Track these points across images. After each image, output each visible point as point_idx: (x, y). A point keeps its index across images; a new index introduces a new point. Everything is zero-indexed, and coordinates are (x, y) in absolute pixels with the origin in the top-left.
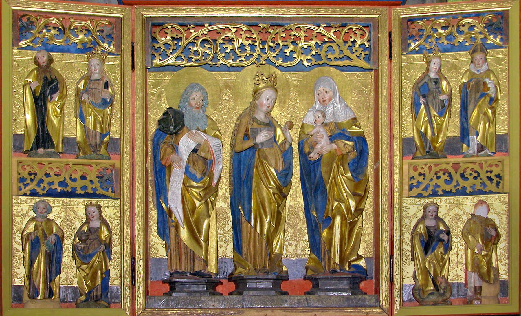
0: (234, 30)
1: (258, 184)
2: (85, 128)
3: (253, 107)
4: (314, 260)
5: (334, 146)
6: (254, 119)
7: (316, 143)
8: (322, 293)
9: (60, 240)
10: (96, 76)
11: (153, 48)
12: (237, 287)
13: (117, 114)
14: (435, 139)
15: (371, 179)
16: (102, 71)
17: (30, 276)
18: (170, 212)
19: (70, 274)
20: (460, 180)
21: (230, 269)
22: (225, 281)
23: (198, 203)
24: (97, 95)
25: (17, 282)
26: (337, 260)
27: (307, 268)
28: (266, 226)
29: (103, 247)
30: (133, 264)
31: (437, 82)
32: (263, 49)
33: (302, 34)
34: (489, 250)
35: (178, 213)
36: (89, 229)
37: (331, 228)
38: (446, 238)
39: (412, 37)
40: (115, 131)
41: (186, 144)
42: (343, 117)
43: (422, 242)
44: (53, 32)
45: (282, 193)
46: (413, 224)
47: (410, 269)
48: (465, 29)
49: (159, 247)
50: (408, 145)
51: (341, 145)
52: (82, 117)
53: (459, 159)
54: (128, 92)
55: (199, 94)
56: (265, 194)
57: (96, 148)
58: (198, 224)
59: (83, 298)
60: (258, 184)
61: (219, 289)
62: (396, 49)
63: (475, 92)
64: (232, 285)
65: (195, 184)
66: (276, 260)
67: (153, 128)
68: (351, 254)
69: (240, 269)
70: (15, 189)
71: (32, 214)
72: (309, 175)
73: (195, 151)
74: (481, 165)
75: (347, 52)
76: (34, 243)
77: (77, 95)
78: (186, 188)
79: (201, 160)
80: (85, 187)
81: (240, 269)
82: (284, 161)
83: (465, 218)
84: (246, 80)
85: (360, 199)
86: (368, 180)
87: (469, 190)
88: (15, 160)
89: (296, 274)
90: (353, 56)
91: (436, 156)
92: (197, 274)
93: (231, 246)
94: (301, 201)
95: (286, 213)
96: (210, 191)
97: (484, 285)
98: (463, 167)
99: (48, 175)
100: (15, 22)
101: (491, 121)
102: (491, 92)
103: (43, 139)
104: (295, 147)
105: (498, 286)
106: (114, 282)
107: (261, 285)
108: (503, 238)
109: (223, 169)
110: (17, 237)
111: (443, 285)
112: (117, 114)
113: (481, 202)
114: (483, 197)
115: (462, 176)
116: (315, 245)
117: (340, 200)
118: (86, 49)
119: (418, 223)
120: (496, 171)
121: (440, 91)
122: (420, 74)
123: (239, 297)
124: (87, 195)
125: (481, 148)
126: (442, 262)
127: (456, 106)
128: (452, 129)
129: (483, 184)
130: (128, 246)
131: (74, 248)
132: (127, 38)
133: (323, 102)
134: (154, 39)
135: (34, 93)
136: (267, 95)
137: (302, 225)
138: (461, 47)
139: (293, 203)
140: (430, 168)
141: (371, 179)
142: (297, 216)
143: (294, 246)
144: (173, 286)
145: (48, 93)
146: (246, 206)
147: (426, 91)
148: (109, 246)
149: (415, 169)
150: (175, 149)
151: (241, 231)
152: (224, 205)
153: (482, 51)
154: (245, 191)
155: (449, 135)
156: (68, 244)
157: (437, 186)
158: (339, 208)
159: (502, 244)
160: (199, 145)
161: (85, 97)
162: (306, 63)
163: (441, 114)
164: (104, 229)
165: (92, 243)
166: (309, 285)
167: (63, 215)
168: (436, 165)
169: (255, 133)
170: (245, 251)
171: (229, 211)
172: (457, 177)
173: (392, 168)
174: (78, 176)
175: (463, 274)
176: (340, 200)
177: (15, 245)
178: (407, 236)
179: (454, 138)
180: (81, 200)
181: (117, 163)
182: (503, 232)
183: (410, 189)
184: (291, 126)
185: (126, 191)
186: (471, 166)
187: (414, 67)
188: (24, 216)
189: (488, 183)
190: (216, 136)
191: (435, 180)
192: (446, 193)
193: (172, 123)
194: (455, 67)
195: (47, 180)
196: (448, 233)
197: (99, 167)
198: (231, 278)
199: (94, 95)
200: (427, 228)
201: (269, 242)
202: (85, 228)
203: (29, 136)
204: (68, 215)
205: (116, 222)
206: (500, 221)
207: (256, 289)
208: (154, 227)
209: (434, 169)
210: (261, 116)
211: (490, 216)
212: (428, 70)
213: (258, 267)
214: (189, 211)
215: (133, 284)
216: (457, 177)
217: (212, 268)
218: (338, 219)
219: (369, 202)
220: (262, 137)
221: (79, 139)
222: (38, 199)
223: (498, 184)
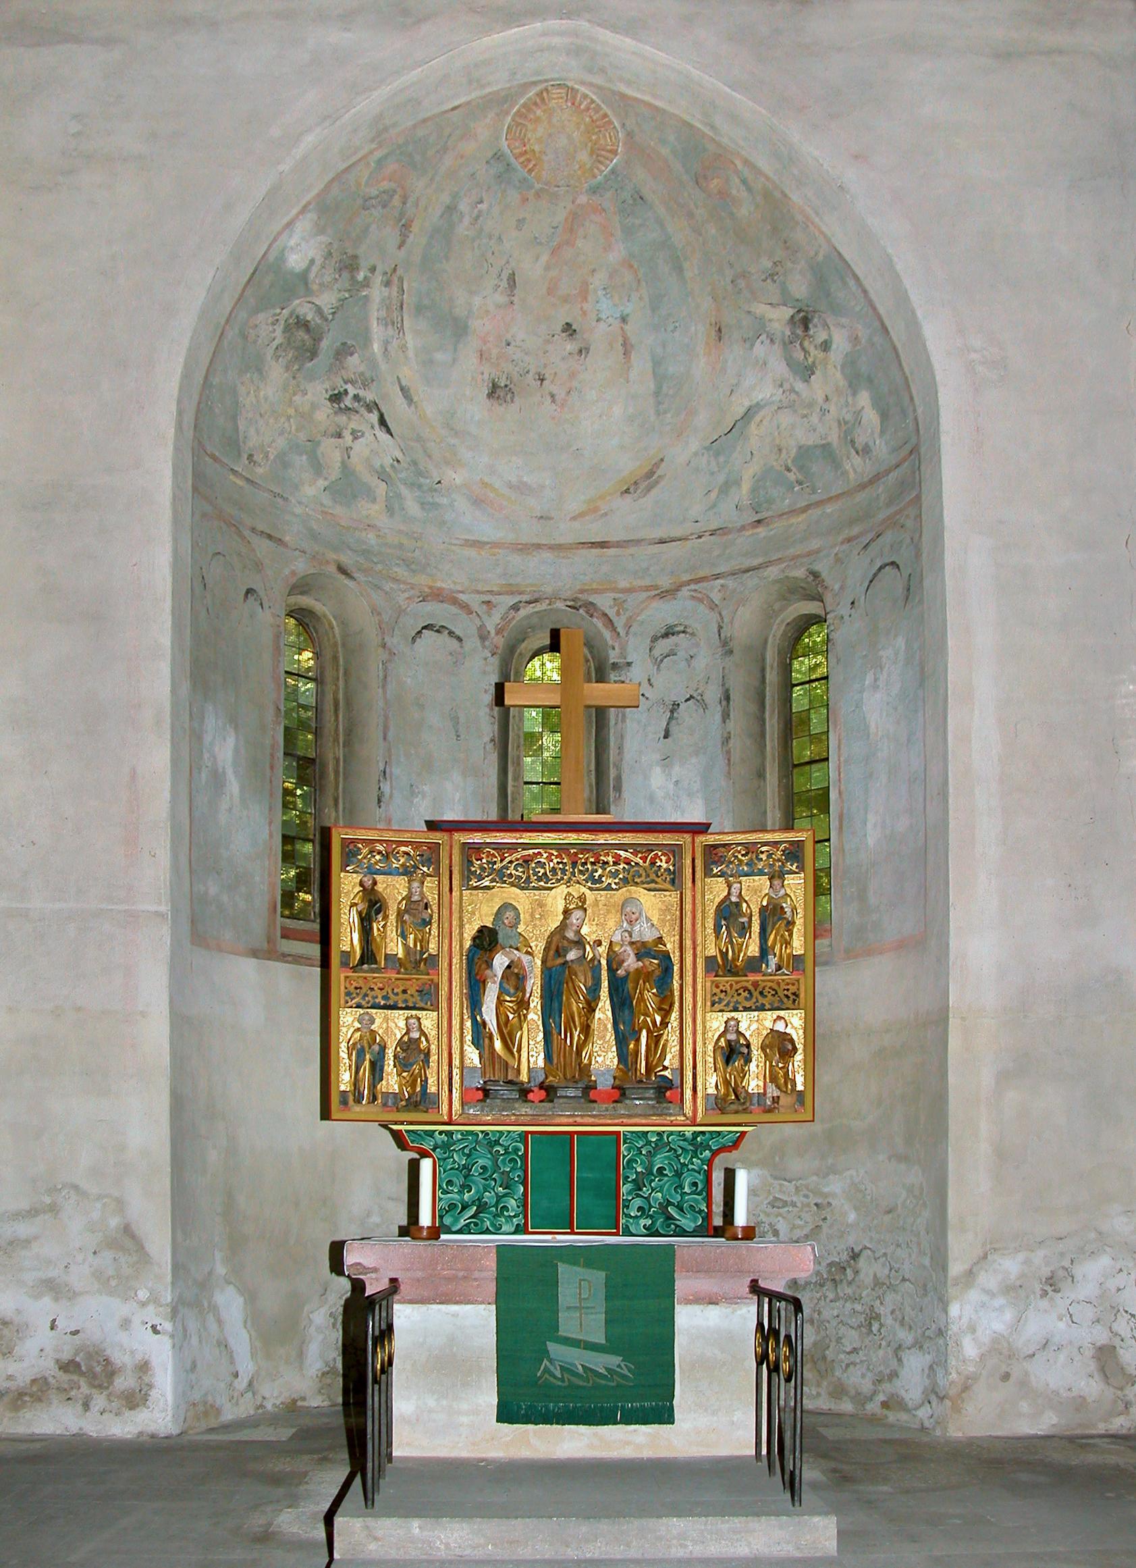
0: (545, 855)
1: (568, 999)
2: (405, 945)
3: (563, 926)
4: (621, 1070)
5: (640, 964)
6: (564, 938)
7: (623, 961)
8: (628, 1102)
9: (383, 1048)
10: (415, 898)
11: (467, 875)
12: (548, 1095)
13: (434, 931)
14: (736, 958)
15: (677, 993)
16: (422, 893)
17: (356, 1083)
18: (484, 1024)
19: (392, 1082)
20: (760, 997)
21: (541, 1079)
22: (536, 1089)
23: (511, 1016)
24: (416, 914)
25: (343, 1088)
26: (643, 1071)
27: (615, 1078)
28: (576, 1038)
29: (422, 1056)
30: (450, 1073)
31: (738, 905)
32: (573, 874)
33: (610, 859)
34: (786, 1063)
35: (492, 1025)
36: (410, 1039)
37: (638, 1040)
38: (746, 1051)
39: (715, 863)
40: (433, 947)
41: (500, 962)
42: (649, 936)
43: (723, 1054)
44: (378, 857)
45: (591, 1008)
46: (716, 1037)
47: (713, 1079)
48: (764, 857)
49: (473, 1056)
50: (710, 961)
51: (647, 963)
52: (404, 936)
53: (759, 978)
54: (446, 912)
55: (512, 914)
56: (575, 1009)
57: (417, 964)
58: (512, 1036)
59: (404, 1103)
60: (568, 999)
61: (531, 1096)
62: (699, 875)
63: (773, 914)
64: (543, 1092)
65: (508, 998)
66: (585, 1070)
67: (468, 944)
68: (657, 1066)
69: (551, 1078)
70: (342, 1002)
71: (357, 1025)
72: (617, 990)
73: (509, 967)
74: (779, 984)
75: (653, 876)
76: (358, 1051)
77: (398, 915)
78: (500, 1002)
79: (515, 977)
80: (406, 1001)
81: (551, 1078)
82: (593, 977)
83: (765, 1033)
84: (556, 899)
85: (666, 1014)
86: (672, 994)
87: (767, 1006)
88: (342, 976)
89: (605, 1083)
90: (659, 880)
91: (736, 974)
92: (510, 1082)
93: (542, 1055)
94: (610, 1014)
95: (595, 1025)
96: (523, 1004)
97: (782, 1096)
98: (762, 984)
99: (372, 989)
100: (343, 848)
101: (788, 943)
102: (789, 914)
103: (368, 956)
104: (604, 962)
105: (795, 1096)
106: (432, 1089)
107: (571, 1093)
108: (800, 1051)
109: (534, 985)
110: (343, 1046)
111: (743, 1095)
112: (434, 931)
113: (779, 1018)
114: (782, 1013)
115: (761, 993)
116: (622, 1056)
117: (646, 1015)
118: (406, 872)
119: (720, 1036)
120: (793, 989)
121: (742, 915)
122: (722, 897)
123: (550, 1104)
124: (407, 1008)
125: (779, 968)
126: (743, 1074)
127: (756, 927)
128: (753, 949)
129: (781, 1001)
130: (446, 1055)
131: (395, 1057)
132: (445, 862)
133: (630, 922)
134: (471, 863)
135: (360, 913)
136: (576, 916)
137: (610, 1036)
138: (761, 873)
139: (601, 1016)
140: (731, 986)
141: (677, 993)
142: (606, 1028)
143: (603, 1057)
144: (486, 1093)
145: (373, 913)
146: (557, 1019)
147: (728, 913)
148: (428, 1054)
149: (717, 987)
150: (489, 965)
151: (552, 1043)
152: (536, 1018)
153: (779, 877)
154: (556, 1005)
155: (749, 954)
156: (390, 1053)
157: (737, 1002)
158: (645, 1021)
159: (799, 1057)
160: (512, 962)
161: (406, 917)
162: (614, 886)
163: (742, 935)
164: (423, 1039)
165: (412, 1052)
166: (617, 1093)
167: (385, 1025)
168: (737, 983)
169: (566, 952)
170: (555, 1061)
171: (540, 1023)
172: (756, 994)
173: (693, 984)
174: (399, 990)
175: (761, 1084)
176: (646, 1015)
177: (342, 1054)
178: (710, 1048)
179: (754, 957)
180: (401, 1012)
181: (435, 978)
182: (800, 1047)
183: (713, 1005)
184: (599, 943)
185: (443, 1005)
186: (769, 984)
187: (716, 890)
188: (349, 1027)
189: (785, 1000)
190: (528, 953)
191: (736, 998)
192: (746, 1009)
193: (486, 941)
194: (755, 891)
195: (371, 993)
196: (748, 1046)
197: (419, 982)
198: (541, 1086)
199: (414, 916)
200: (729, 1042)
201: (579, 1053)
202: (406, 1039)
203: (355, 952)
204: (392, 1026)
205: (434, 1033)
206: (798, 1035)
207: (567, 1097)
208: (469, 1038)
209: (735, 987)
210: (570, 935)
211: (788, 1031)
212: (729, 893)
213: (568, 1077)
214: (503, 1023)
215: (450, 1091)
216: (756, 994)
217: (524, 1077)
218: (644, 1033)
219: (674, 1015)
220: (572, 955)
221: (400, 956)
222: (361, 1011)
223: (794, 1001)
